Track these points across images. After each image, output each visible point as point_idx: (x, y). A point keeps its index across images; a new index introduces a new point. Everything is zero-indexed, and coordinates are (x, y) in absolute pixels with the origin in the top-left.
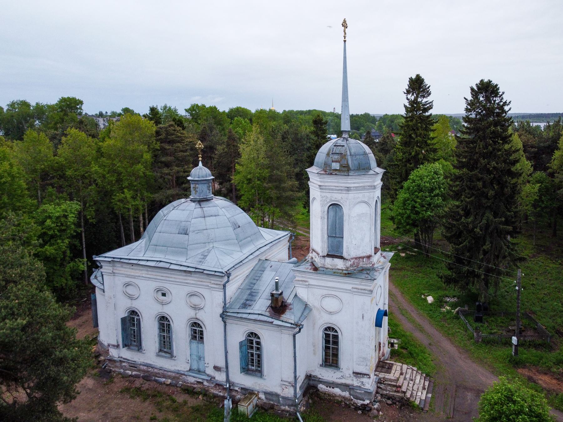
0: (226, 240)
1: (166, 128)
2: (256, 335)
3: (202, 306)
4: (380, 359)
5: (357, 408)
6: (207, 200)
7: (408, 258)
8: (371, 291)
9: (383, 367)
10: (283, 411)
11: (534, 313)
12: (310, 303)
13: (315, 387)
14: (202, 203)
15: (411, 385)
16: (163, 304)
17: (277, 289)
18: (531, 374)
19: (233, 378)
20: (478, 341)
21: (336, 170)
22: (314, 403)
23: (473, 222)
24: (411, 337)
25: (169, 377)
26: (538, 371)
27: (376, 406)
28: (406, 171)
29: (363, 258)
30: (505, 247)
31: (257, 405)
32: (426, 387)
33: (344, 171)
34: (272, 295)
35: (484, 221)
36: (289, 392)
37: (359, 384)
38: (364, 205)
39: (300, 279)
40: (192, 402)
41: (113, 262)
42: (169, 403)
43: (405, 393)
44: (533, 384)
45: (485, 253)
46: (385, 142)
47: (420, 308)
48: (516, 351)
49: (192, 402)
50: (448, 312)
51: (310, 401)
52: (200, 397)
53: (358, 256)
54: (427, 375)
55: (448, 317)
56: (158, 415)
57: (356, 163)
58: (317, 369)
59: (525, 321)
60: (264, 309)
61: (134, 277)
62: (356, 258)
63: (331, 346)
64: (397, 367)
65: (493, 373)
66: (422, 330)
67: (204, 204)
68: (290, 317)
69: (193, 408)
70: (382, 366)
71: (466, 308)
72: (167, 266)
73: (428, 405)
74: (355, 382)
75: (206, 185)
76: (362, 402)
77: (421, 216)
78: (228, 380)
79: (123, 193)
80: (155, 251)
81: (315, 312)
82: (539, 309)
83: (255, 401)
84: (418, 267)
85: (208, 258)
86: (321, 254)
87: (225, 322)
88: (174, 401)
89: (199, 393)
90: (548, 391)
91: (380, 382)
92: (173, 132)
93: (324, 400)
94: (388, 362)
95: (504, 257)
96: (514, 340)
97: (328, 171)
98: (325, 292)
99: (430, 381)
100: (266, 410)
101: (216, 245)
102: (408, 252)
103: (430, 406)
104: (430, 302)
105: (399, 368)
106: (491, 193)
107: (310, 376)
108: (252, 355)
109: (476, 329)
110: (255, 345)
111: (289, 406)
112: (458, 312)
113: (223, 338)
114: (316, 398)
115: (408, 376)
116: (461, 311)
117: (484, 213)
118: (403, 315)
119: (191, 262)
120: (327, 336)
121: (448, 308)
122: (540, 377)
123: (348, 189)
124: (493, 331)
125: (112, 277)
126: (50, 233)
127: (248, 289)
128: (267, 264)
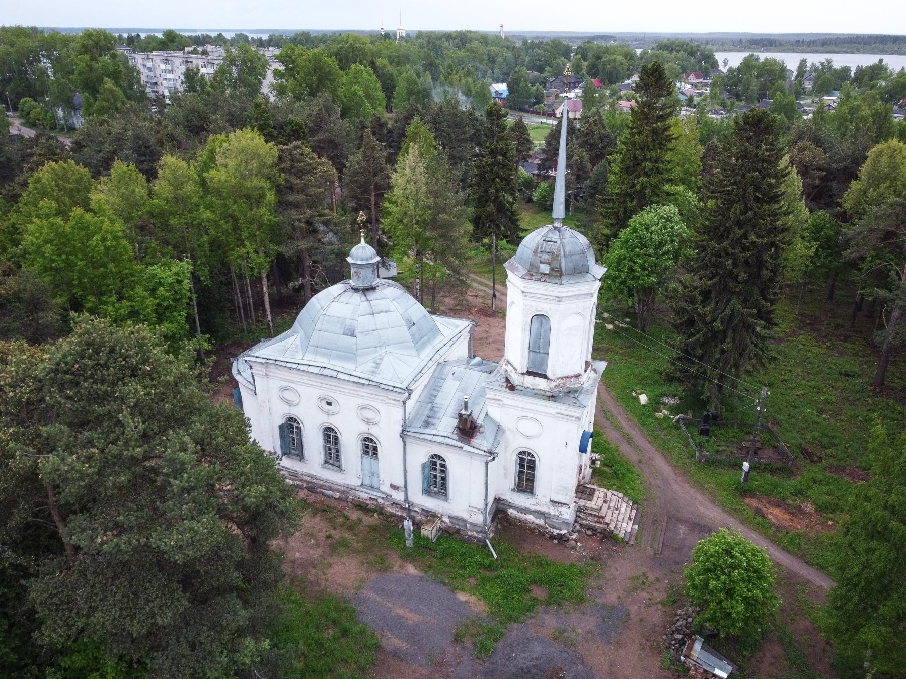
0: (400, 343)
1: (291, 151)
2: (440, 457)
3: (376, 420)
4: (579, 482)
5: (552, 537)
6: (373, 288)
7: (616, 333)
8: (579, 419)
9: (583, 493)
10: (470, 536)
11: (776, 423)
12: (504, 424)
13: (505, 512)
14: (368, 293)
15: (615, 515)
16: (328, 413)
17: (466, 408)
18: (760, 506)
19: (411, 498)
20: (700, 461)
21: (545, 274)
22: (503, 528)
23: (713, 311)
24: (617, 451)
25: (338, 491)
26: (769, 503)
27: (574, 537)
28: (625, 211)
29: (571, 377)
30: (751, 346)
31: (440, 528)
32: (633, 517)
33: (555, 277)
34: (461, 416)
35: (728, 312)
36: (478, 519)
37: (557, 513)
38: (578, 317)
39: (493, 397)
40: (368, 520)
41: (267, 363)
42: (342, 519)
43: (608, 524)
44: (760, 518)
45: (723, 352)
46: (591, 131)
47: (629, 410)
48: (746, 480)
49: (368, 520)
50: (666, 418)
51: (499, 526)
52: (376, 515)
53: (565, 375)
54: (634, 503)
55: (665, 425)
56: (333, 532)
57: (571, 265)
58: (508, 494)
59: (765, 436)
60: (451, 430)
61: (293, 382)
62: (562, 378)
63: (526, 471)
64: (600, 493)
65: (713, 502)
66: (630, 441)
67: (371, 295)
68: (482, 441)
69: (369, 526)
70: (583, 491)
71: (690, 416)
72: (334, 374)
73: (633, 538)
74: (552, 511)
75: (371, 270)
76: (558, 531)
77: (640, 281)
78: (406, 500)
79: (244, 247)
80: (316, 353)
81: (508, 434)
82: (786, 418)
83: (438, 524)
84: (629, 347)
85: (381, 367)
86: (519, 371)
87: (404, 442)
88: (347, 518)
89: (374, 511)
90: (777, 528)
91: (580, 510)
92: (301, 157)
93: (515, 525)
94: (589, 486)
95: (750, 358)
96: (746, 465)
97: (533, 273)
98: (522, 414)
99: (637, 510)
100: (451, 534)
101: (388, 349)
102: (617, 323)
103: (636, 539)
104: (643, 402)
105: (602, 495)
106: (743, 276)
107: (499, 499)
108: (435, 477)
109: (700, 446)
110: (438, 467)
111: (477, 532)
112: (678, 421)
113: (402, 458)
114: (505, 523)
115: (612, 505)
116: (683, 420)
117: (730, 300)
118: (607, 419)
119: (363, 369)
120: (522, 460)
121: (666, 412)
122: (770, 510)
123: (559, 299)
124: (721, 448)
125: (265, 380)
126: (165, 304)
127: (428, 403)
128: (448, 369)
